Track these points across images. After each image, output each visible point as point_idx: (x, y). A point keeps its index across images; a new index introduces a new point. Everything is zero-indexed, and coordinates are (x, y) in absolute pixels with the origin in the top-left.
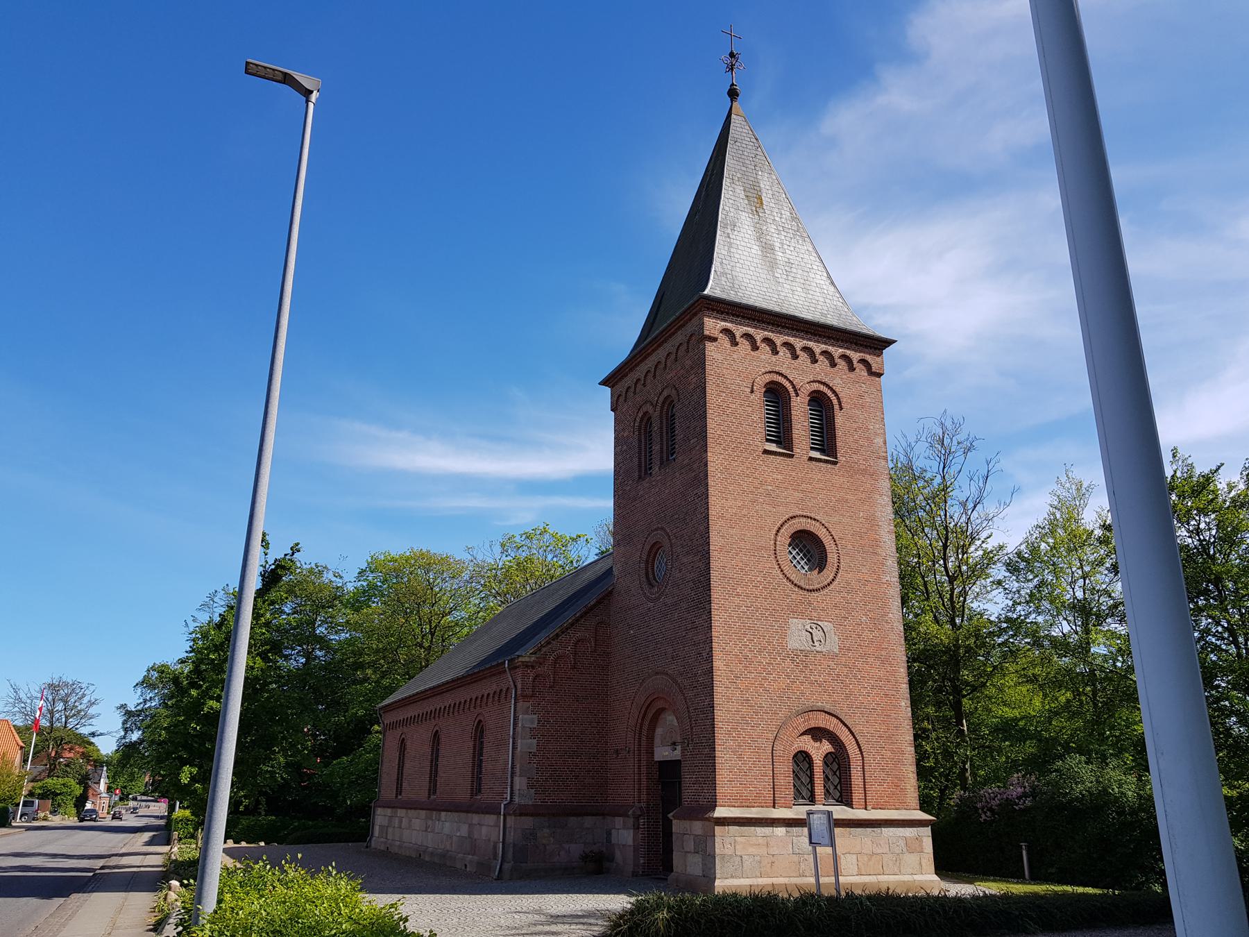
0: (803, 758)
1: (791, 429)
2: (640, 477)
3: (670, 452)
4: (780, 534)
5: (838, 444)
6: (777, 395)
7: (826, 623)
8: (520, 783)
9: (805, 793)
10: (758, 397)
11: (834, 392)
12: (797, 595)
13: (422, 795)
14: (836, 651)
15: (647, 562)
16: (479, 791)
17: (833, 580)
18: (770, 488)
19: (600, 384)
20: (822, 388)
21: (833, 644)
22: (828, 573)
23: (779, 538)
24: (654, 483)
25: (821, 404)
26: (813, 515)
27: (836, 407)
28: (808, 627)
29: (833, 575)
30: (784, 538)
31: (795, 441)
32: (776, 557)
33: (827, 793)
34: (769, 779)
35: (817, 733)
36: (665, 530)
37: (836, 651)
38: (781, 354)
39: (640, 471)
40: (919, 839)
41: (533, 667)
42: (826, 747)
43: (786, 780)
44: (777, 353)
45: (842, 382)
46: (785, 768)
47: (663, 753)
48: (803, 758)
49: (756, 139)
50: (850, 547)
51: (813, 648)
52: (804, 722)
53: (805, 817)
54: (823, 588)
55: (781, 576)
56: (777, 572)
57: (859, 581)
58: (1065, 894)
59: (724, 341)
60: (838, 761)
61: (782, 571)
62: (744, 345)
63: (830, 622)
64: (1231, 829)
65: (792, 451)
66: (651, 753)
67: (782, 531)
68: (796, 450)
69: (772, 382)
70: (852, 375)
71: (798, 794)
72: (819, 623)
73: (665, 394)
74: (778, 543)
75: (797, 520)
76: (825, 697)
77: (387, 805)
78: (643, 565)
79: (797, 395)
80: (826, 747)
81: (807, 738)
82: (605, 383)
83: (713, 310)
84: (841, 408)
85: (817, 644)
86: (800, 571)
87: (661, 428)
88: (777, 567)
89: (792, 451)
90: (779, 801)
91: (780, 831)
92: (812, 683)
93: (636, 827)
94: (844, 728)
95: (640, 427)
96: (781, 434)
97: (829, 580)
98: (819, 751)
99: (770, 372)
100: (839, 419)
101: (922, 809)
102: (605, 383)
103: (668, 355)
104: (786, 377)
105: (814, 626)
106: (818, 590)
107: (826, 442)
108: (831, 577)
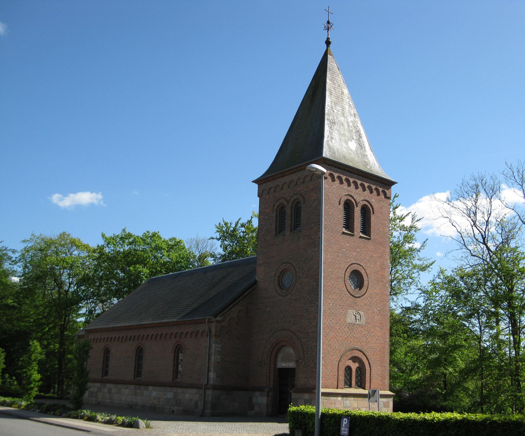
0: (348, 369)
1: (354, 222)
2: (276, 235)
3: (296, 225)
4: (347, 271)
5: (372, 230)
6: (348, 207)
7: (362, 312)
8: (212, 375)
9: (348, 383)
10: (341, 207)
11: (371, 205)
12: (351, 299)
13: (130, 376)
14: (364, 324)
15: (279, 277)
16: (177, 377)
17: (365, 293)
18: (344, 250)
19: (252, 182)
20: (367, 203)
21: (363, 322)
22: (364, 290)
23: (346, 273)
24: (286, 240)
25: (366, 212)
26: (360, 263)
27: (372, 213)
28: (355, 314)
29: (365, 290)
30: (348, 274)
31: (355, 228)
32: (345, 282)
33: (357, 383)
34: (336, 377)
35: (355, 359)
36: (292, 264)
37: (364, 324)
38: (352, 186)
39: (276, 231)
40: (388, 402)
41: (220, 323)
42: (357, 365)
43: (342, 378)
44: (350, 186)
45: (375, 200)
46: (342, 373)
47: (282, 365)
48: (348, 369)
49: (339, 69)
50: (373, 278)
51: (356, 323)
52: (350, 354)
53: (380, 399)
54: (362, 296)
55: (346, 291)
56: (345, 289)
57: (375, 293)
58: (409, 420)
59: (329, 179)
60: (361, 371)
61: (346, 288)
62: (337, 182)
63: (363, 311)
64: (390, 364)
65: (353, 233)
66: (275, 364)
67: (348, 270)
68: (355, 233)
69: (348, 200)
70: (378, 197)
71: (346, 383)
72: (359, 312)
73: (295, 197)
74: (346, 275)
75: (354, 265)
76: (359, 344)
77: (95, 381)
78: (277, 278)
79: (357, 206)
80: (357, 365)
81: (351, 361)
82: (255, 182)
83: (326, 164)
84: (373, 213)
85: (357, 321)
86: (351, 287)
87: (291, 213)
88: (345, 286)
89: (353, 233)
90: (340, 386)
91: (340, 398)
92: (354, 338)
93: (268, 396)
94: (365, 357)
95: (277, 210)
96: (349, 224)
97: (364, 293)
98: (354, 366)
99: (347, 195)
100: (373, 218)
101: (390, 390)
102: (255, 182)
103: (298, 179)
104: (353, 198)
105: (357, 313)
106: (359, 297)
107: (366, 229)
108: (365, 292)
